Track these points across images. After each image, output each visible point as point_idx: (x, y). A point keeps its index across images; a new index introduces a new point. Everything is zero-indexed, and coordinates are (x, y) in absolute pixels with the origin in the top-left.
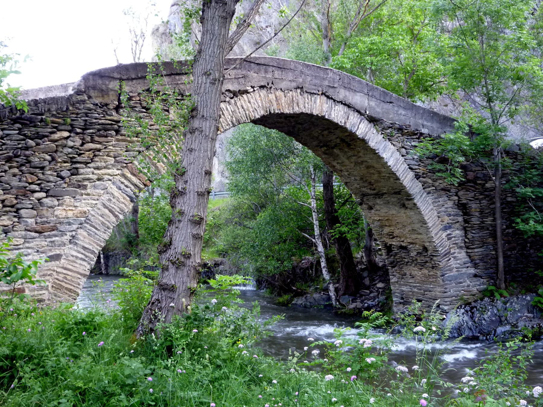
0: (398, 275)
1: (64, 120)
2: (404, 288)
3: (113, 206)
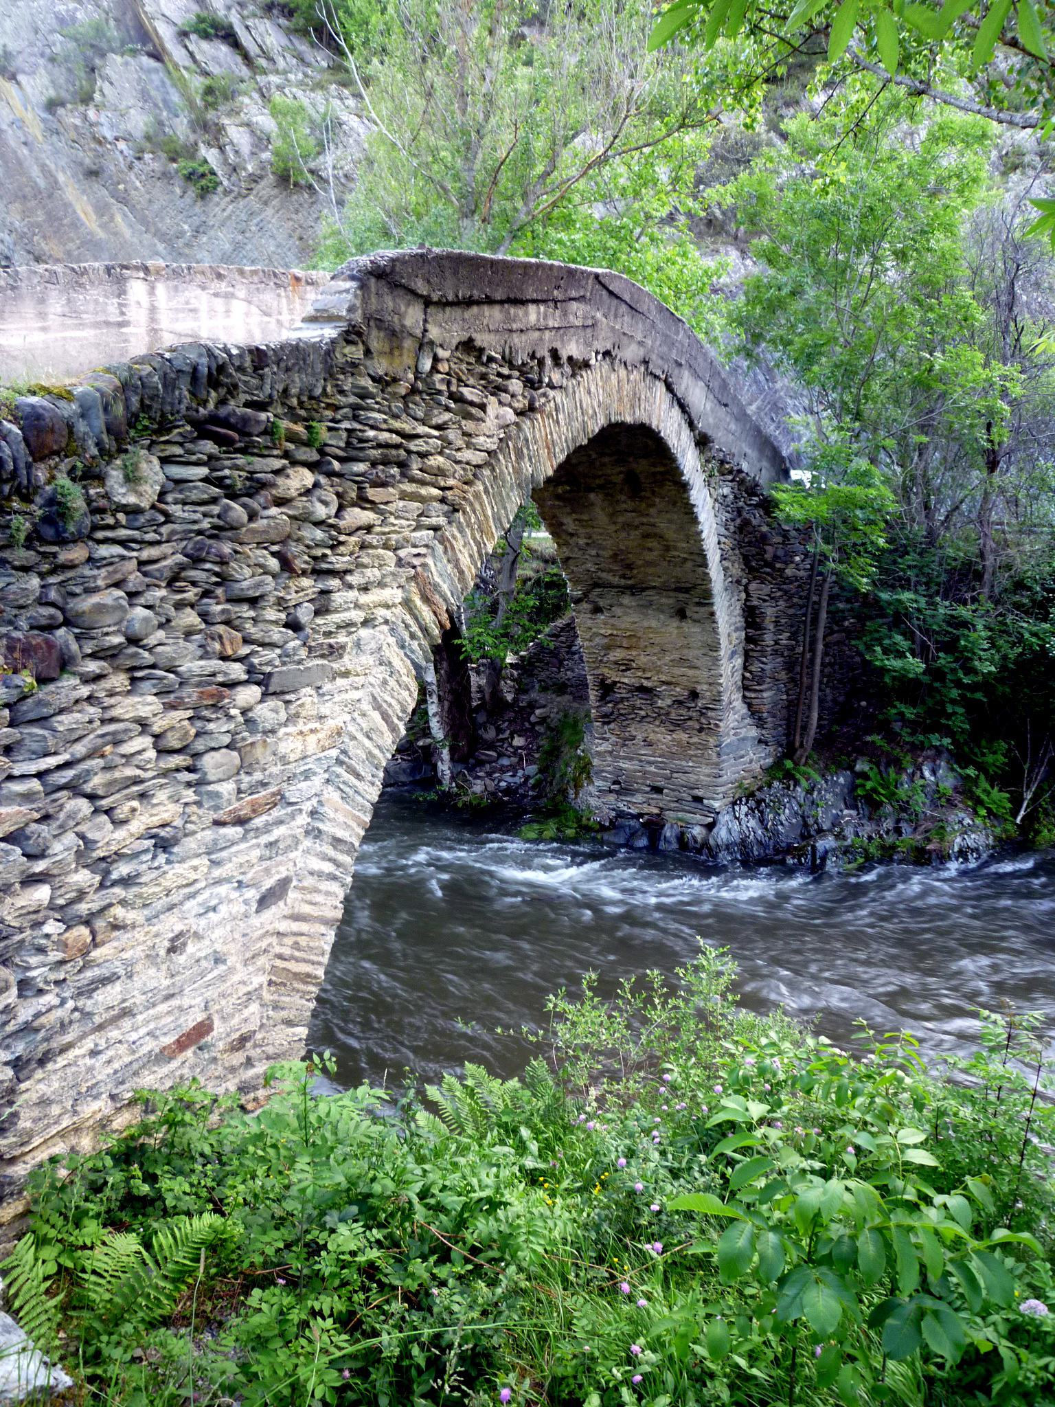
0: (614, 738)
1: (308, 428)
2: (625, 765)
3: (389, 699)
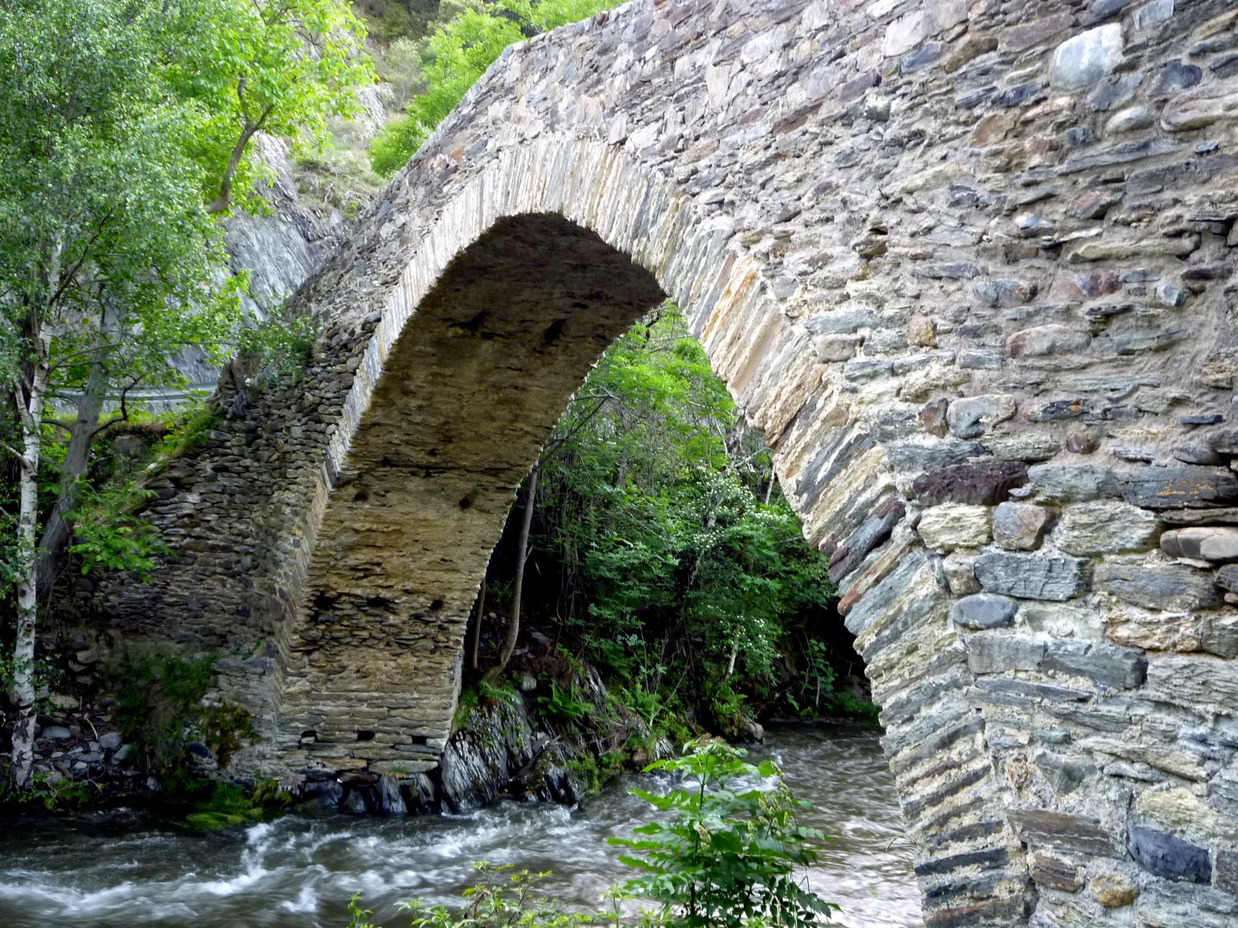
2: (328, 707)
